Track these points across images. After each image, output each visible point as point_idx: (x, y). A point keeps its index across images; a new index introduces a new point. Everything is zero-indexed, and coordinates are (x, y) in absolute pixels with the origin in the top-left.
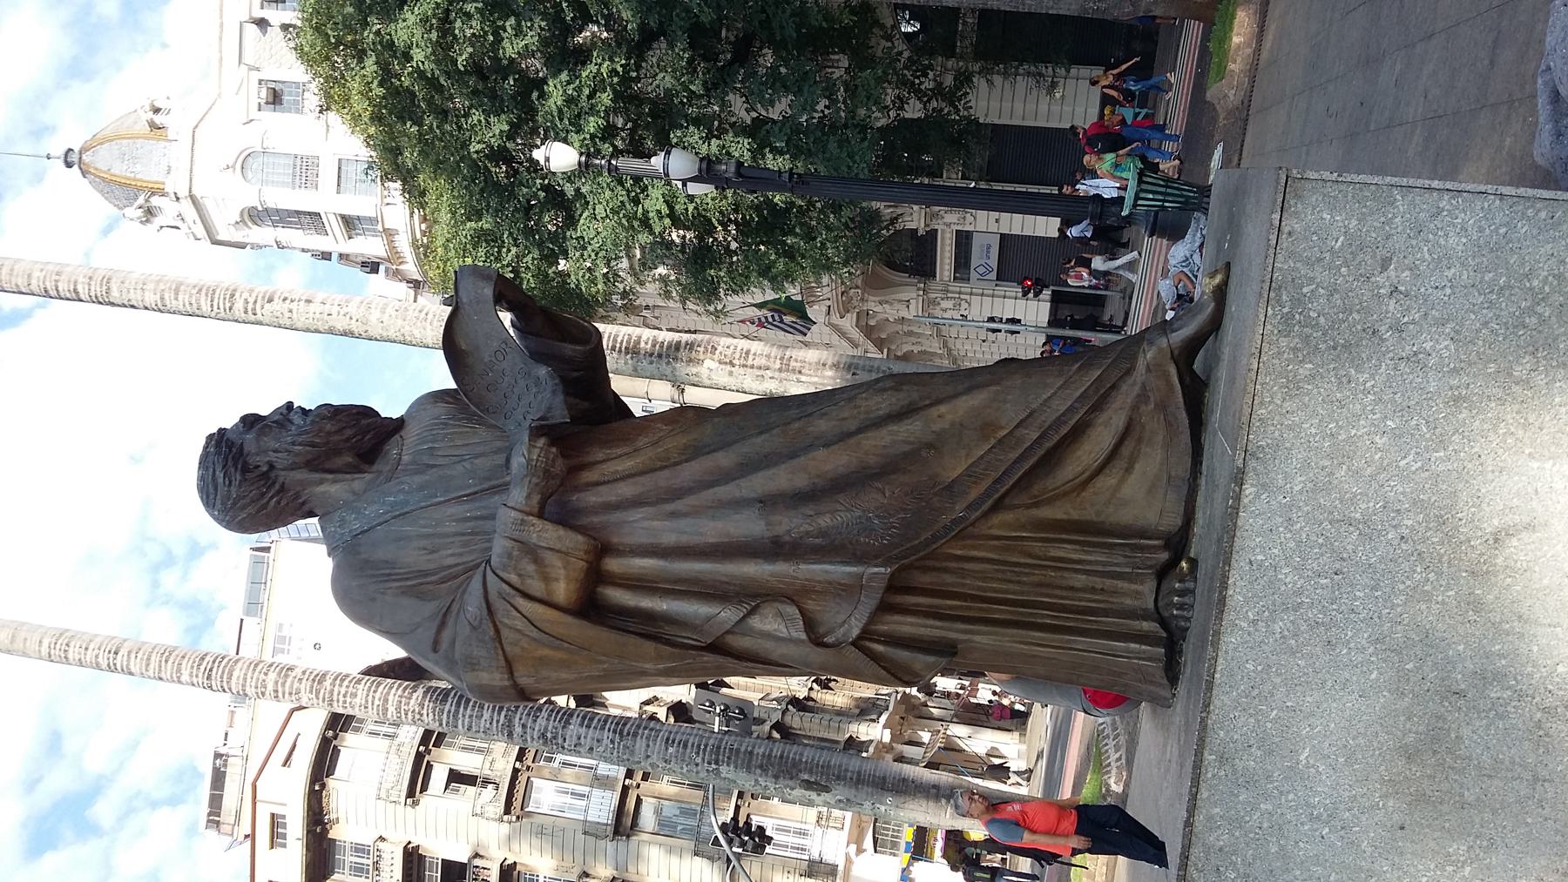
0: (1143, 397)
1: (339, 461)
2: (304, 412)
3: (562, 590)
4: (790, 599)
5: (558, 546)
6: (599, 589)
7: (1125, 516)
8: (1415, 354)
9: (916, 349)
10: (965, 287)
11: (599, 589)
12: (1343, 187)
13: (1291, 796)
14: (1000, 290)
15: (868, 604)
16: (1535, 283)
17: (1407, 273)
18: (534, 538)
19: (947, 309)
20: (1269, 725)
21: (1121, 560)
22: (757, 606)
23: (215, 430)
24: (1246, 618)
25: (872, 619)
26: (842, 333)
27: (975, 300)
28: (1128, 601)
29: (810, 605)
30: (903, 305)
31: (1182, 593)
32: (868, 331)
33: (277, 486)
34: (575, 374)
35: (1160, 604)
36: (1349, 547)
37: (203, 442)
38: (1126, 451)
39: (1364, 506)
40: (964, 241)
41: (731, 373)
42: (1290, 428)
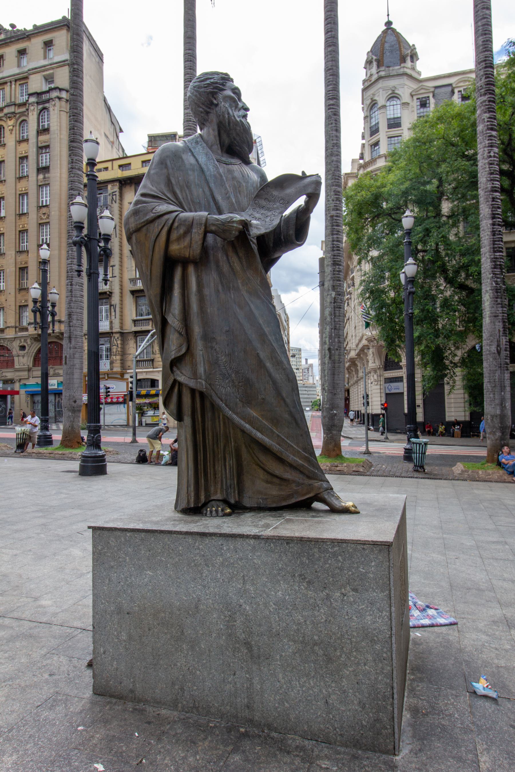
0: (299, 484)
1: (224, 137)
2: (245, 116)
3: (174, 248)
4: (188, 349)
5: (193, 242)
6: (180, 264)
7: (247, 483)
8: (318, 606)
9: (359, 368)
10: (382, 382)
11: (180, 264)
12: (387, 570)
13: (133, 569)
14: (384, 395)
15: (192, 383)
16: (355, 653)
17: (352, 600)
18: (194, 230)
19: (373, 377)
20: (159, 558)
21: (228, 484)
22: (182, 335)
23: (231, 77)
24: (200, 545)
25: (186, 386)
26: (360, 341)
27: (378, 387)
28: (212, 489)
29: (187, 358)
30: (373, 361)
31: (217, 511)
32: (362, 350)
33: (208, 110)
34: (282, 238)
35: (213, 502)
36: (234, 584)
37: (224, 72)
38: (275, 480)
39: (252, 589)
40: (399, 379)
41: (331, 303)
42: (280, 556)
